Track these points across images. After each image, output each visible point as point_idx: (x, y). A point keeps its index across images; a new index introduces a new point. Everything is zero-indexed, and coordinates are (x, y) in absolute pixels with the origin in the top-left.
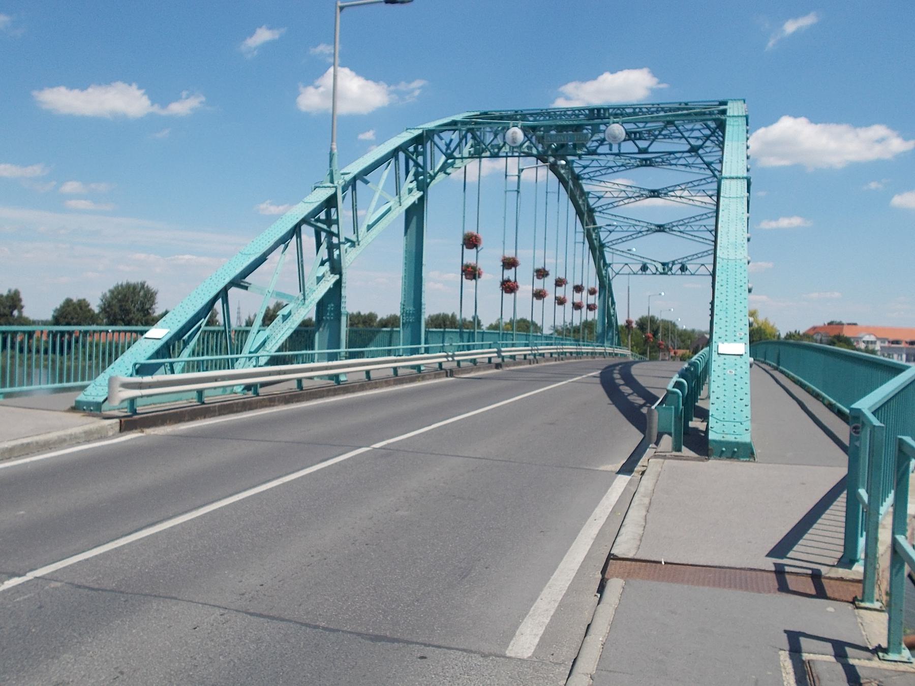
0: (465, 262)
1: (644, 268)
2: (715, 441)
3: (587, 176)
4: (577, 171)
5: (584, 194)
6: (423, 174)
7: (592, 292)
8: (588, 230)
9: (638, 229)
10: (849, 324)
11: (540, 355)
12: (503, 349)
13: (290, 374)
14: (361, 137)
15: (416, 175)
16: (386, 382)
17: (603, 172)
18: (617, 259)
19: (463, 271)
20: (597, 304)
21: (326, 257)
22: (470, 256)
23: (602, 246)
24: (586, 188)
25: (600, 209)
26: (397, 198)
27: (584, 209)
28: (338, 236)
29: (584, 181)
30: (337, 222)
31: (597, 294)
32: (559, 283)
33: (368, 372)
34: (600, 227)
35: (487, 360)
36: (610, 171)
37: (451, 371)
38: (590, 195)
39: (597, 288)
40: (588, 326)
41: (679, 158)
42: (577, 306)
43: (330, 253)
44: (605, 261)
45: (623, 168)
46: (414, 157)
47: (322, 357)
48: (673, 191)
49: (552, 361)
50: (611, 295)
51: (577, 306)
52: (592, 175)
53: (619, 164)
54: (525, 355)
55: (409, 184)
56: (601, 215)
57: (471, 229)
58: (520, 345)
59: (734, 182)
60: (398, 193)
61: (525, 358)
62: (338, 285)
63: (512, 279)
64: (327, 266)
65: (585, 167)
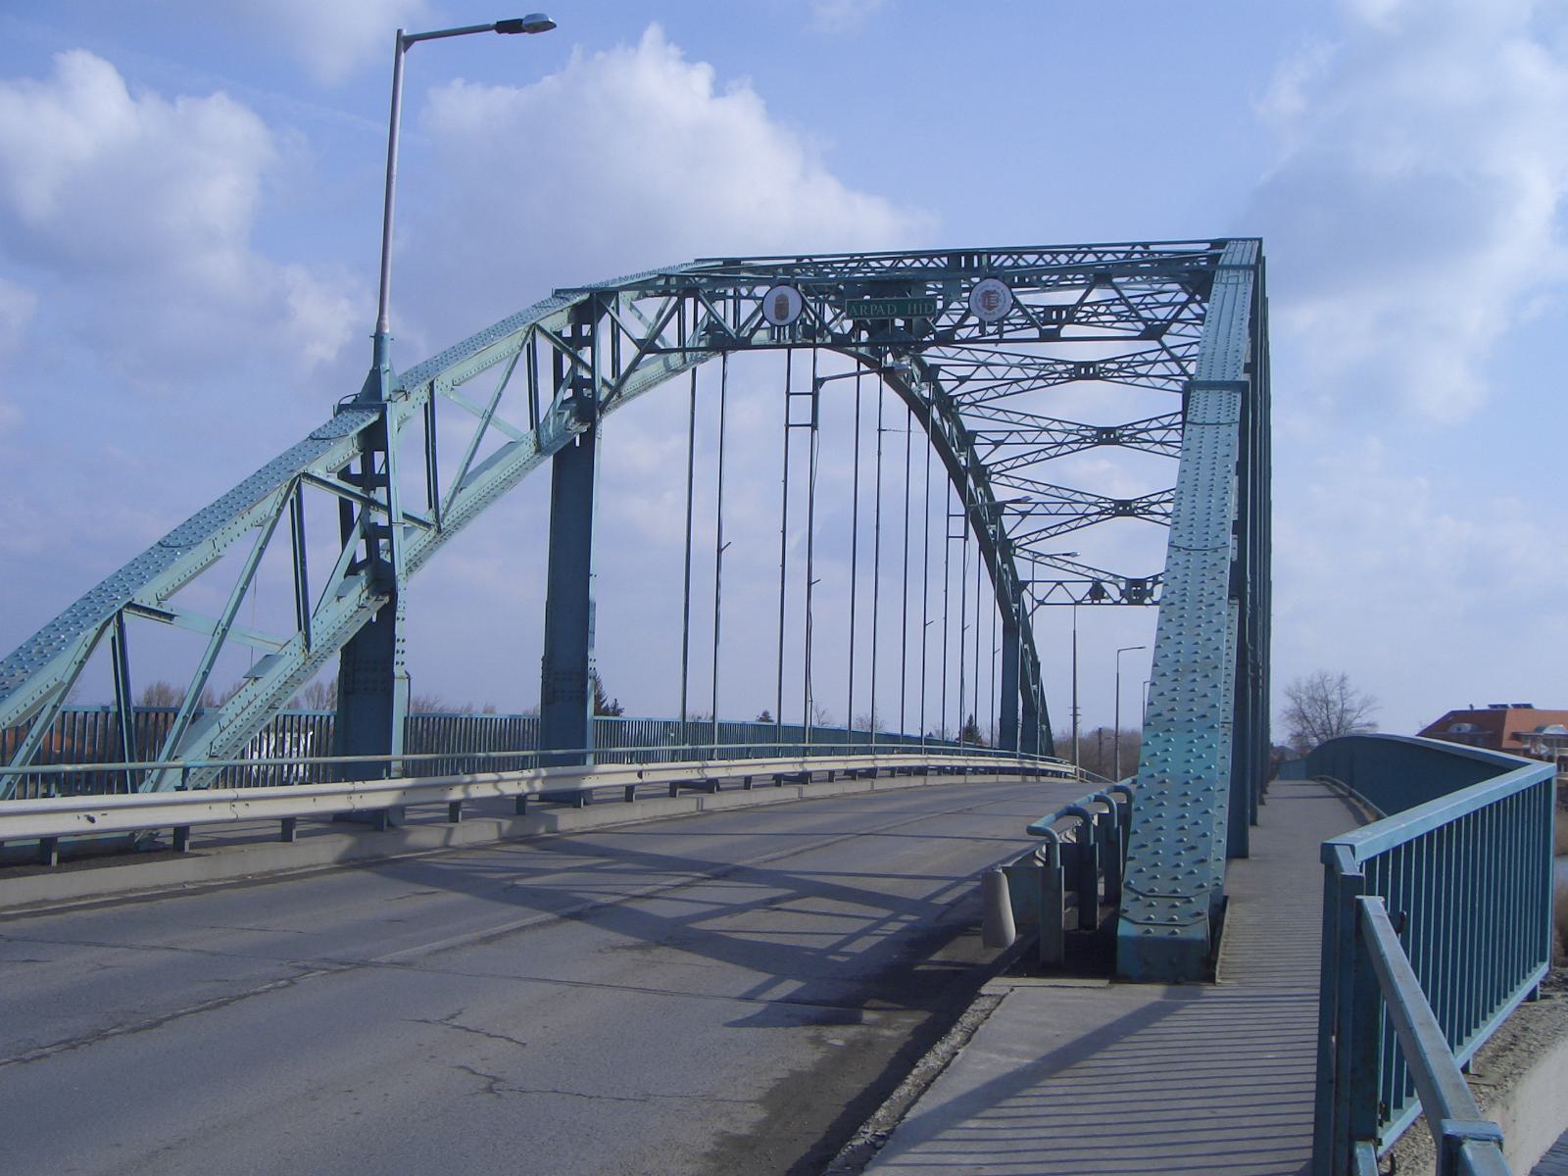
1: (1097, 592)
2: (1127, 939)
3: (967, 399)
4: (947, 387)
9: (1080, 508)
10: (1517, 706)
14: (584, 334)
17: (1001, 390)
18: (1042, 572)
21: (362, 556)
25: (999, 468)
28: (388, 508)
30: (384, 480)
34: (1003, 504)
36: (1015, 388)
38: (978, 440)
41: (1155, 362)
43: (372, 549)
45: (1040, 383)
48: (1146, 430)
52: (978, 396)
56: (1003, 480)
59: (1213, 395)
62: (388, 614)
65: (962, 380)
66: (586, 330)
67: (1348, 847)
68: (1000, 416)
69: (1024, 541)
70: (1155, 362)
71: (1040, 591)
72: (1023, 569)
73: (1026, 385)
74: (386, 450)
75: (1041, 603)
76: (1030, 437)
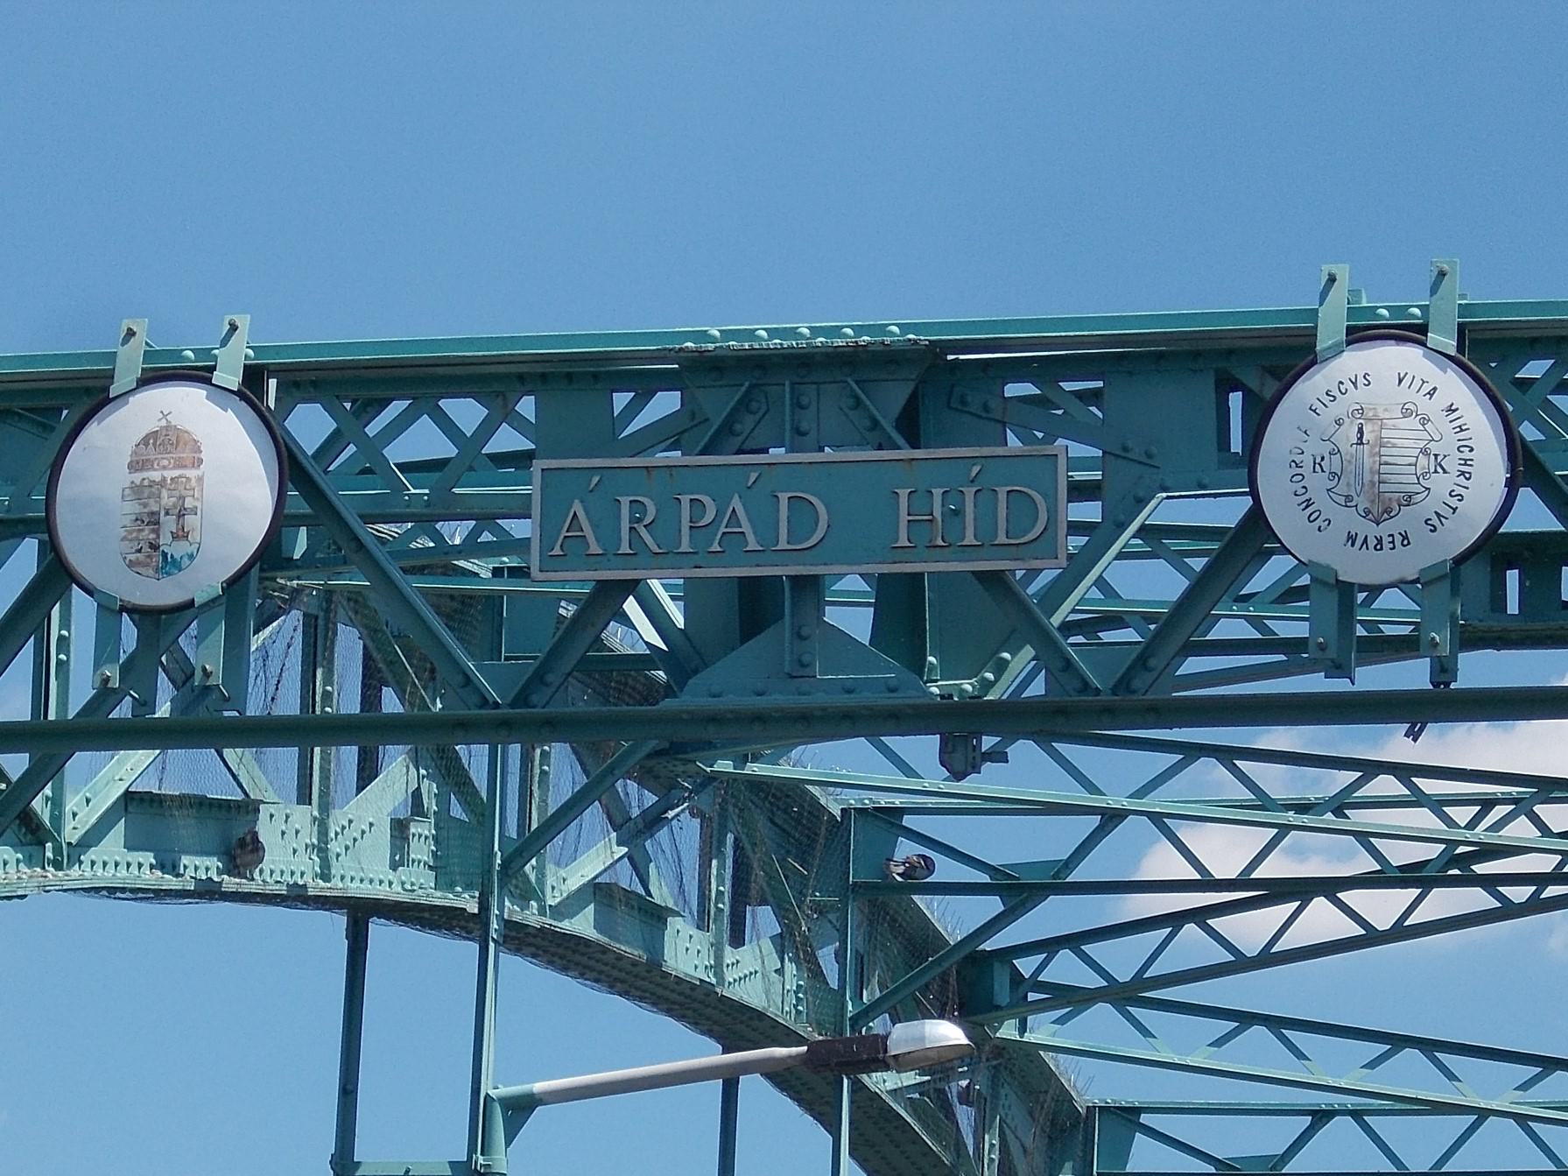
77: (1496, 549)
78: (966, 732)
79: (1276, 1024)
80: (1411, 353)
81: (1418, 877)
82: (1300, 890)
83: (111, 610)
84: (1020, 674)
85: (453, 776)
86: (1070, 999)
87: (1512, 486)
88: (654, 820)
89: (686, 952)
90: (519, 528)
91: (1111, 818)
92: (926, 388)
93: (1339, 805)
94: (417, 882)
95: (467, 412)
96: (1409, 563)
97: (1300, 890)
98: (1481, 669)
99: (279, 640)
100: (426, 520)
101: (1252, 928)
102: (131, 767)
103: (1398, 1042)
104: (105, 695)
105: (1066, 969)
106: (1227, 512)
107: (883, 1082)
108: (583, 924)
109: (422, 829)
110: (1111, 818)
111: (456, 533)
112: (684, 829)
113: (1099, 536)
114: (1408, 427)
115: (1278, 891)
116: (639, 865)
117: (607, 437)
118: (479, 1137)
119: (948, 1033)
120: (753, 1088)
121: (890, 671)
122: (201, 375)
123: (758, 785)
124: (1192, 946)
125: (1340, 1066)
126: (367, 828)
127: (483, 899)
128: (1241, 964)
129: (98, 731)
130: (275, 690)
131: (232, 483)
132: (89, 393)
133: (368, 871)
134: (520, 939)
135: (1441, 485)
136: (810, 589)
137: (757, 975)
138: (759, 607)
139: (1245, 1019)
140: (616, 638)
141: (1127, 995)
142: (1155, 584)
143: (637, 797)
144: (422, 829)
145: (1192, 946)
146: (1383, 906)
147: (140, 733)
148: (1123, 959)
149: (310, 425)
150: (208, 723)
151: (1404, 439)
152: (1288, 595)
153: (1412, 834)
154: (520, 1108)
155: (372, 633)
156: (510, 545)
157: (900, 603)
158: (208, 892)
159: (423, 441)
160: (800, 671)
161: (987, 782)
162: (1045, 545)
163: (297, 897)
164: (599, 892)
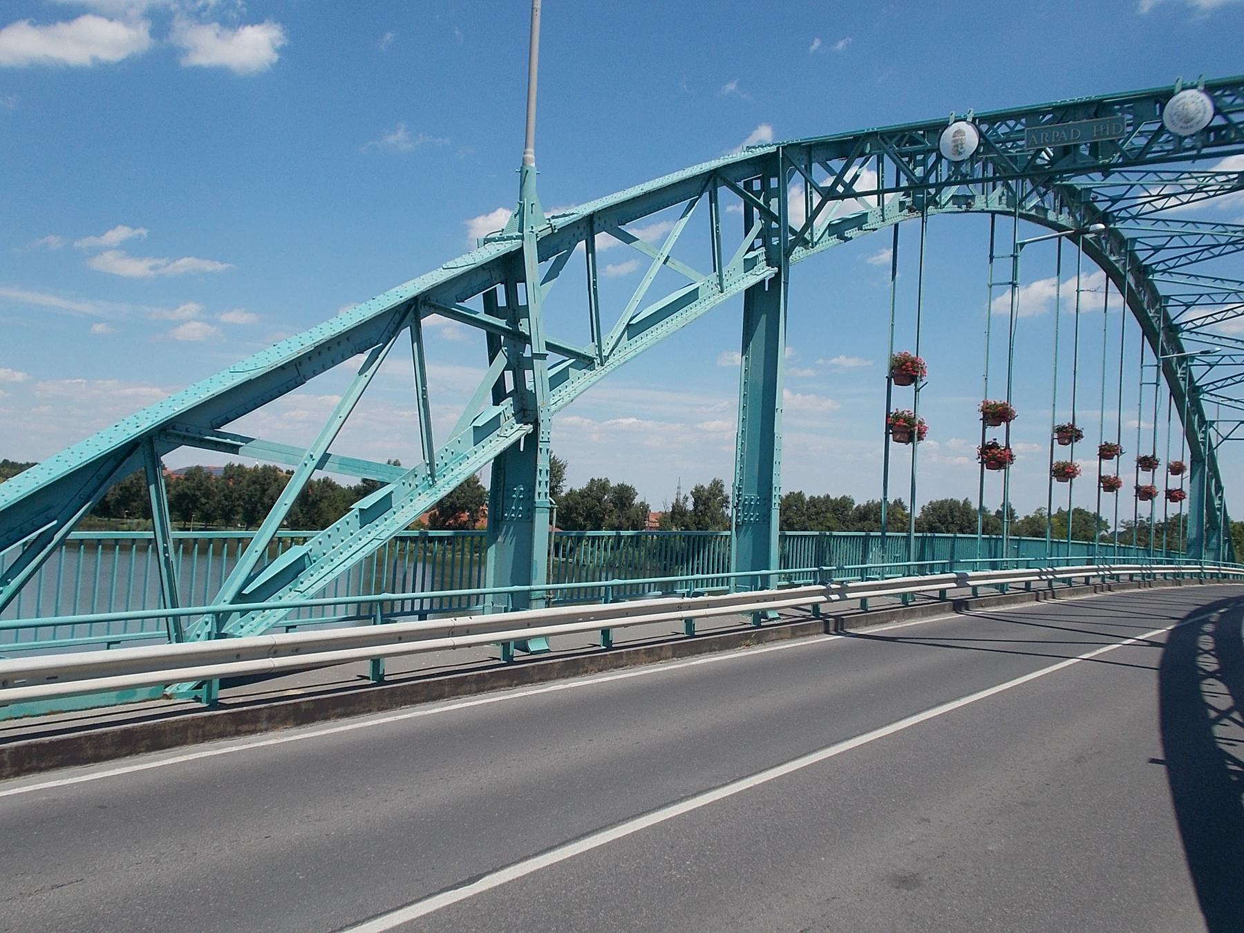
0: (893, 410)
3: (1162, 267)
4: (1141, 256)
5: (1156, 298)
6: (777, 233)
7: (1176, 469)
8: (1167, 363)
11: (1112, 576)
12: (971, 574)
13: (419, 642)
15: (764, 235)
16: (649, 652)
18: (1226, 413)
19: (888, 427)
20: (1186, 489)
22: (903, 398)
23: (1196, 390)
24: (1163, 289)
25: (1190, 325)
26: (713, 277)
27: (1159, 325)
29: (1157, 276)
30: (525, 312)
31: (1187, 473)
32: (1107, 452)
33: (605, 632)
34: (1192, 357)
35: (1083, 580)
36: (1206, 254)
37: (838, 619)
39: (1187, 463)
40: (1173, 526)
41: (1226, 244)
42: (1145, 493)
44: (1202, 416)
46: (761, 201)
47: (742, 584)
49: (1086, 592)
50: (1215, 474)
51: (1145, 493)
53: (1223, 240)
54: (1087, 578)
55: (741, 245)
57: (905, 347)
58: (1079, 562)
60: (717, 266)
61: (1087, 583)
63: (1002, 443)
64: (507, 405)
66: (774, 182)
67: (483, 333)
68: (1192, 280)
69: (1211, 387)
70: (1226, 244)
71: (1224, 429)
72: (1209, 411)
73: (1216, 251)
74: (525, 281)
75: (1226, 439)
76: (1218, 299)
77: (1208, 129)
78: (1106, 171)
79: (1164, 221)
80: (1194, 92)
81: (1193, 192)
82: (1169, 196)
83: (951, 163)
84: (1116, 158)
85: (1008, 187)
86: (1124, 219)
87: (1214, 115)
88: (1045, 193)
89: (1051, 216)
90: (1020, 143)
91: (1132, 186)
92: (1098, 108)
93: (1177, 180)
94: (1003, 207)
95: (1011, 123)
96: (1192, 131)
97: (1169, 196)
98: (1204, 151)
99: (979, 166)
100: (1004, 142)
101: (1159, 204)
102: (953, 190)
103: (1188, 222)
104: (950, 177)
105: (1123, 214)
106: (1155, 127)
107: (1088, 236)
108: (1033, 212)
109: (1004, 198)
110: (1132, 186)
111: (1009, 145)
112: (1051, 195)
113: (1131, 134)
114: (1194, 105)
115: (1165, 196)
116: (1043, 201)
117: (1039, 123)
118: (1015, 250)
119: (1102, 226)
120: (1063, 238)
121: (1092, 159)
122: (964, 120)
123: (1065, 186)
124: (1148, 208)
125: (1177, 228)
126: (995, 198)
127: (1014, 208)
128: (1174, 195)
129: (949, 183)
130: (979, 174)
131: (971, 137)
132: (945, 125)
133: (995, 206)
134: (1021, 216)
135: (1200, 115)
136: (1077, 146)
137: (1064, 219)
138: (1066, 151)
139: (1158, 220)
140: (1039, 161)
141: (1134, 218)
142: (1142, 142)
143: (1042, 190)
144: (1004, 198)
145: (1148, 208)
146: (1185, 198)
147: (955, 183)
148: (1134, 211)
149: (984, 127)
150: (965, 181)
151: (1192, 108)
152: (1167, 142)
153: (1191, 184)
154: (1022, 245)
155: (994, 165)
156: (1018, 146)
157: (1094, 149)
158: (966, 211)
159: (1003, 129)
160: (1075, 161)
161: (1109, 181)
162: (1122, 133)
163: (983, 211)
164: (1035, 206)
